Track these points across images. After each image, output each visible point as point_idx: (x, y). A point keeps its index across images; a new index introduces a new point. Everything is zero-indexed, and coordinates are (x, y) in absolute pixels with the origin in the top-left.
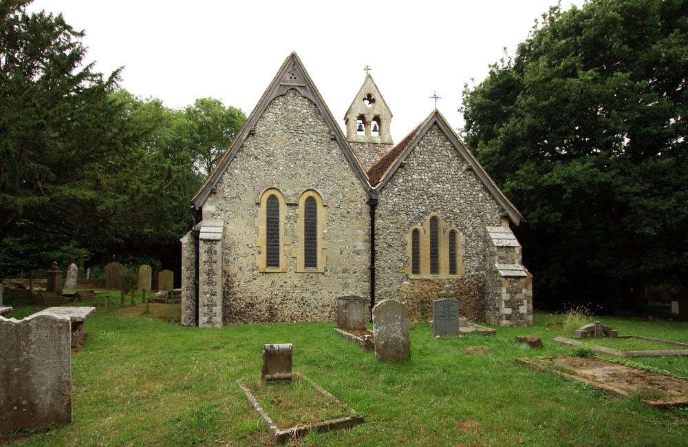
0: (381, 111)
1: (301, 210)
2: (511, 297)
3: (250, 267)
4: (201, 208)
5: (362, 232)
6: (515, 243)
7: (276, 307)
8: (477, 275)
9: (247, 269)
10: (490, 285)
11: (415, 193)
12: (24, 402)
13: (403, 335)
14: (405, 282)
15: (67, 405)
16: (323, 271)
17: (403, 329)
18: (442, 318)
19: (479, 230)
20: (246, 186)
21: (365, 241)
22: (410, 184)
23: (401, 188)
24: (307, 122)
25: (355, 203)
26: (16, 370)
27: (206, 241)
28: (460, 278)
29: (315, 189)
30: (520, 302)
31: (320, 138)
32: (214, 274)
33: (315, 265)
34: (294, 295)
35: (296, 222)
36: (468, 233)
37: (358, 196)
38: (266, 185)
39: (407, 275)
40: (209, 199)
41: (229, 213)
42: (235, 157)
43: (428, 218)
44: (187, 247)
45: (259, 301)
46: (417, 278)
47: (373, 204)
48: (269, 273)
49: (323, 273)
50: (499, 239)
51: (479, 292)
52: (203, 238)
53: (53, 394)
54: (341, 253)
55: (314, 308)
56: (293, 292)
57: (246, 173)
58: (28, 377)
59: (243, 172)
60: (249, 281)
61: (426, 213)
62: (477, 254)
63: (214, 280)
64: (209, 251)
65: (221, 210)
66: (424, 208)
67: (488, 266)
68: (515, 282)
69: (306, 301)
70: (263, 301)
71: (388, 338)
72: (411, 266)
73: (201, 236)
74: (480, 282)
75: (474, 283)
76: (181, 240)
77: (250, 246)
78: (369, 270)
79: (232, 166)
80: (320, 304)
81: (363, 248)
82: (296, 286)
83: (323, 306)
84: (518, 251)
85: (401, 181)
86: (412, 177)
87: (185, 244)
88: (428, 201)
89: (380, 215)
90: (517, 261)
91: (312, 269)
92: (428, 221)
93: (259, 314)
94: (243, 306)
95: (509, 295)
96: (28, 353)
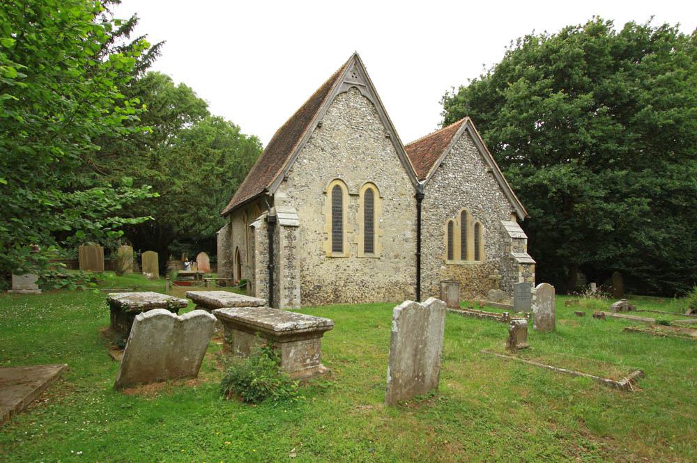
3: (318, 252)
9: (316, 254)
38: (365, 179)
39: (444, 261)
43: (460, 212)
45: (326, 283)
46: (452, 263)
47: (419, 197)
62: (494, 244)
72: (447, 254)
77: (317, 232)
80: (377, 286)
84: (526, 241)
90: (526, 250)
91: (369, 254)
92: (460, 214)
93: (325, 295)
94: (311, 289)
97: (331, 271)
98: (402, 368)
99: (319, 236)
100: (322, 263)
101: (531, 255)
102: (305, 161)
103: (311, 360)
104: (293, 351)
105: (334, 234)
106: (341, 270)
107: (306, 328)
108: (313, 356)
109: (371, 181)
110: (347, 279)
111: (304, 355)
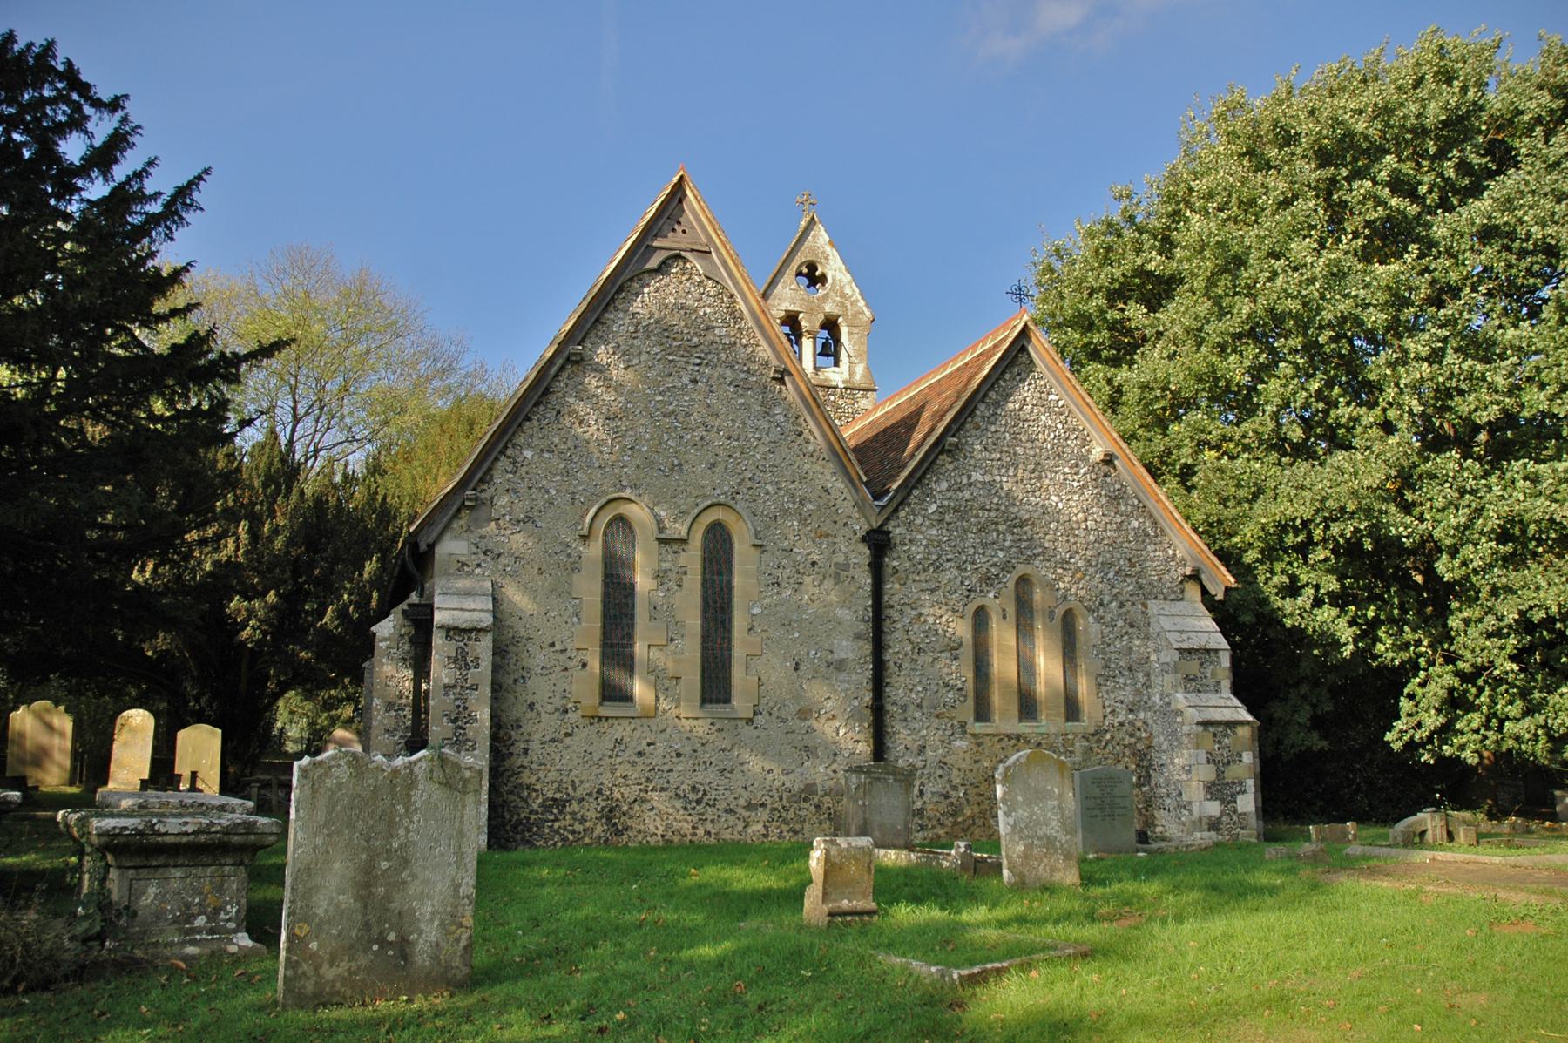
0: (843, 305)
1: (692, 558)
2: (1219, 774)
3: (558, 702)
4: (431, 547)
5: (853, 615)
6: (1218, 641)
7: (625, 808)
8: (1131, 723)
9: (550, 708)
10: (1165, 746)
11: (977, 516)
12: (392, 937)
13: (1064, 829)
14: (958, 743)
15: (465, 948)
16: (751, 716)
17: (1063, 816)
18: (1098, 812)
19: (1133, 610)
20: (553, 492)
21: (858, 636)
22: (967, 495)
23: (946, 503)
24: (710, 337)
25: (831, 539)
26: (384, 865)
27: (451, 631)
28: (1092, 730)
29: (731, 503)
30: (1236, 788)
31: (742, 376)
32: (471, 719)
33: (727, 700)
34: (673, 777)
35: (680, 586)
36: (1108, 617)
37: (840, 523)
38: (704, 496)
39: (963, 725)
40: (455, 525)
41: (503, 560)
42: (528, 419)
43: (1010, 580)
44: (388, 648)
45: (580, 792)
46: (989, 731)
47: (879, 543)
48: (607, 718)
49: (750, 721)
50: (1181, 632)
51: (1138, 765)
52: (445, 622)
53: (442, 922)
54: (796, 669)
55: (726, 811)
56: (671, 770)
57: (554, 459)
58: (404, 883)
59: (546, 455)
60: (553, 740)
61: (1007, 567)
62: (1130, 669)
63: (470, 734)
64: (460, 660)
65: (485, 553)
66: (1001, 554)
67: (1157, 698)
68: (1227, 736)
69: (705, 793)
70: (590, 794)
71: (1032, 837)
72: (970, 702)
73: (438, 617)
74: (1139, 739)
75: (1126, 742)
76: (374, 629)
77: (558, 647)
78: (868, 712)
79: (520, 440)
80: (742, 802)
81: (851, 656)
82: (679, 755)
83: (749, 806)
84: (1225, 660)
85: (944, 485)
86: (969, 477)
87: (385, 639)
88: (1009, 537)
89: (896, 571)
90: (1226, 684)
91: (719, 709)
92: (1011, 585)
93: (578, 827)
94: (535, 806)
95: (1212, 767)
96: (408, 830)
97: (596, 757)
98: (320, 912)
99: (561, 657)
100: (568, 735)
101: (1242, 701)
102: (528, 454)
103: (210, 920)
104: (152, 891)
105: (609, 650)
106: (629, 754)
107: (186, 834)
108: (217, 910)
109: (722, 499)
110: (648, 780)
111: (188, 906)
